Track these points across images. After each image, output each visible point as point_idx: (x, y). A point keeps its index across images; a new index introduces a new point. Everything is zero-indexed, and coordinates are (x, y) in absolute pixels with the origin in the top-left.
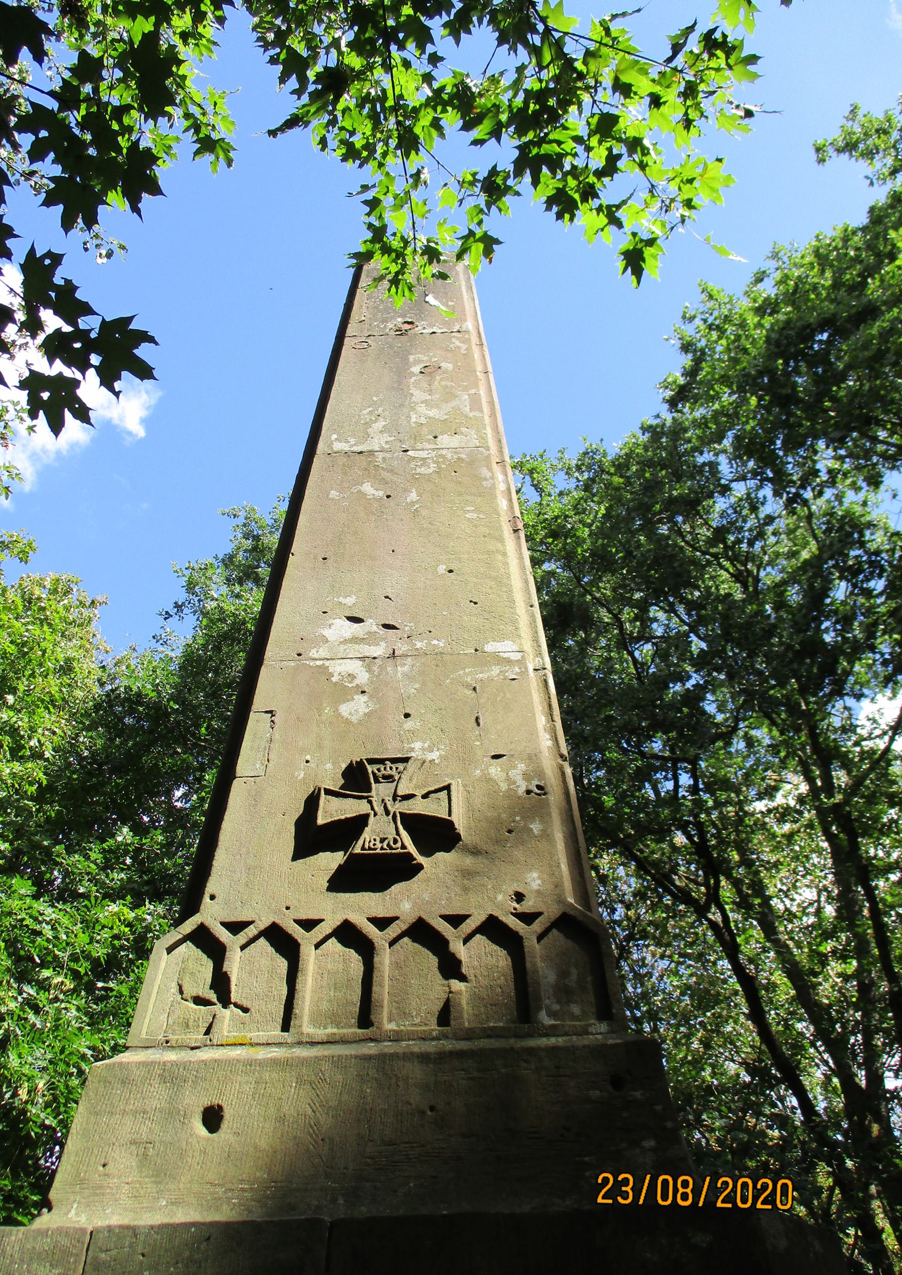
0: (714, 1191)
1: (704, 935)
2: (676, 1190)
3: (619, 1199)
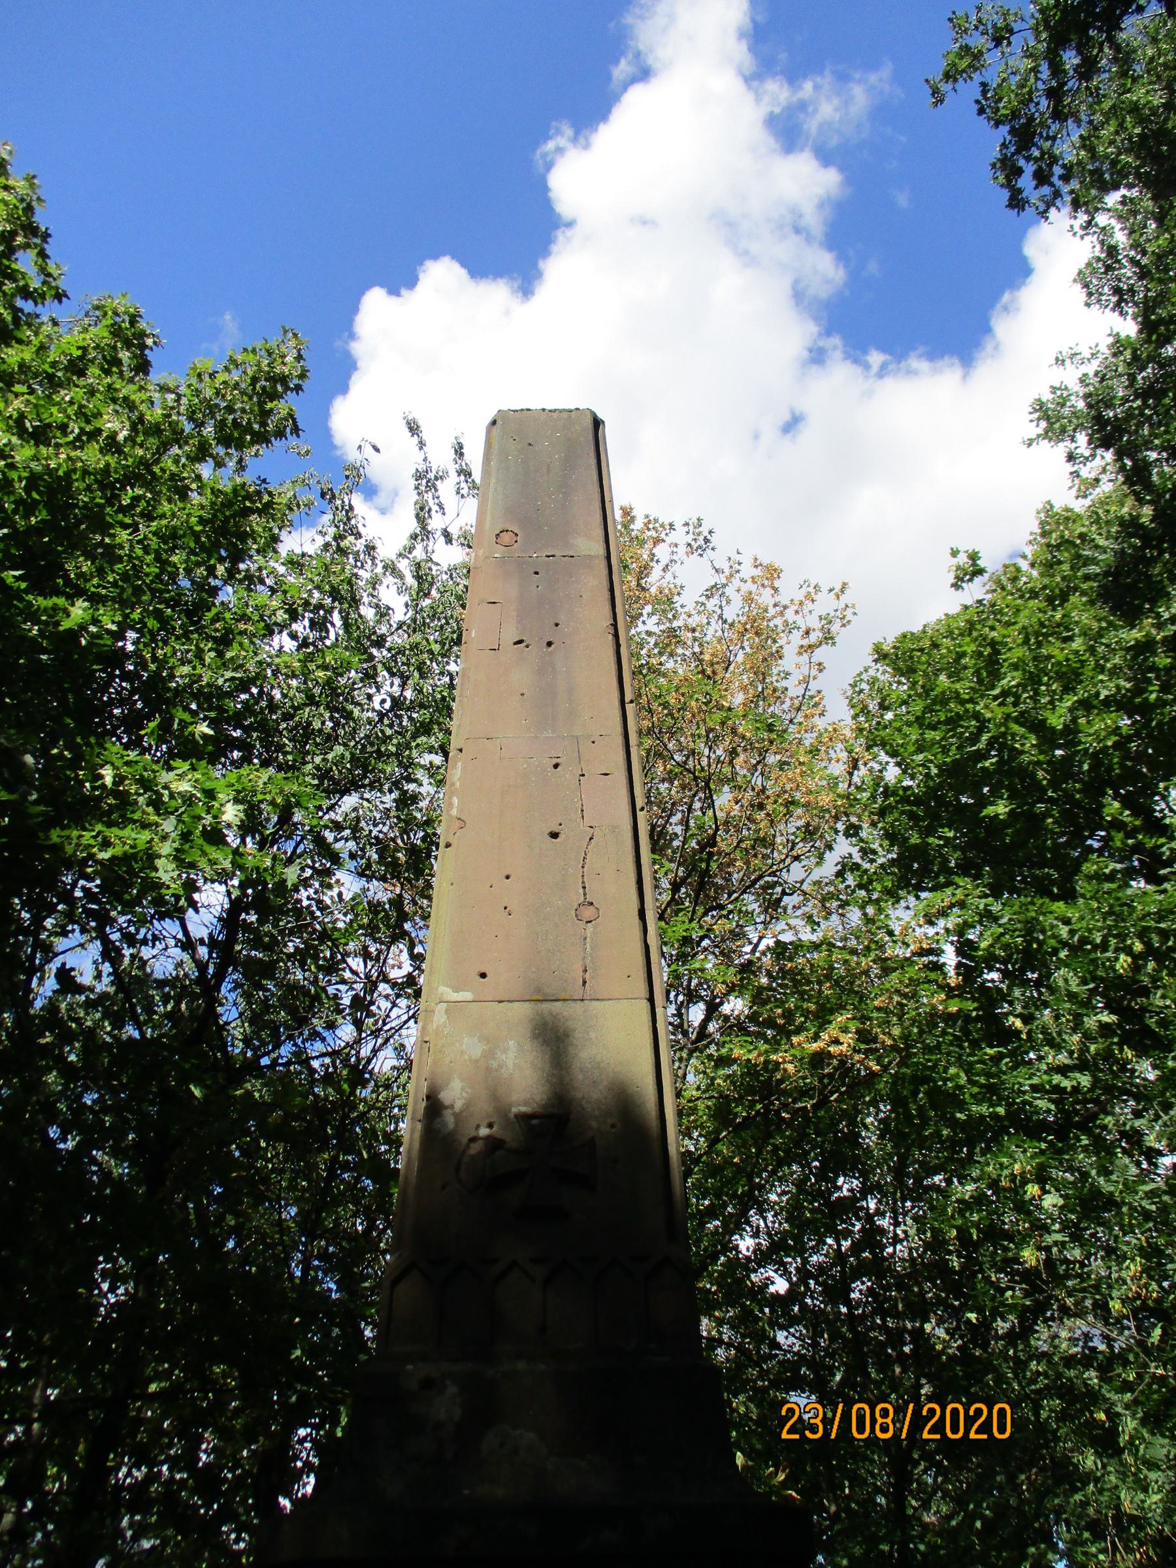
0: (918, 1422)
1: (1066, 980)
2: (873, 1421)
3: (807, 1433)
